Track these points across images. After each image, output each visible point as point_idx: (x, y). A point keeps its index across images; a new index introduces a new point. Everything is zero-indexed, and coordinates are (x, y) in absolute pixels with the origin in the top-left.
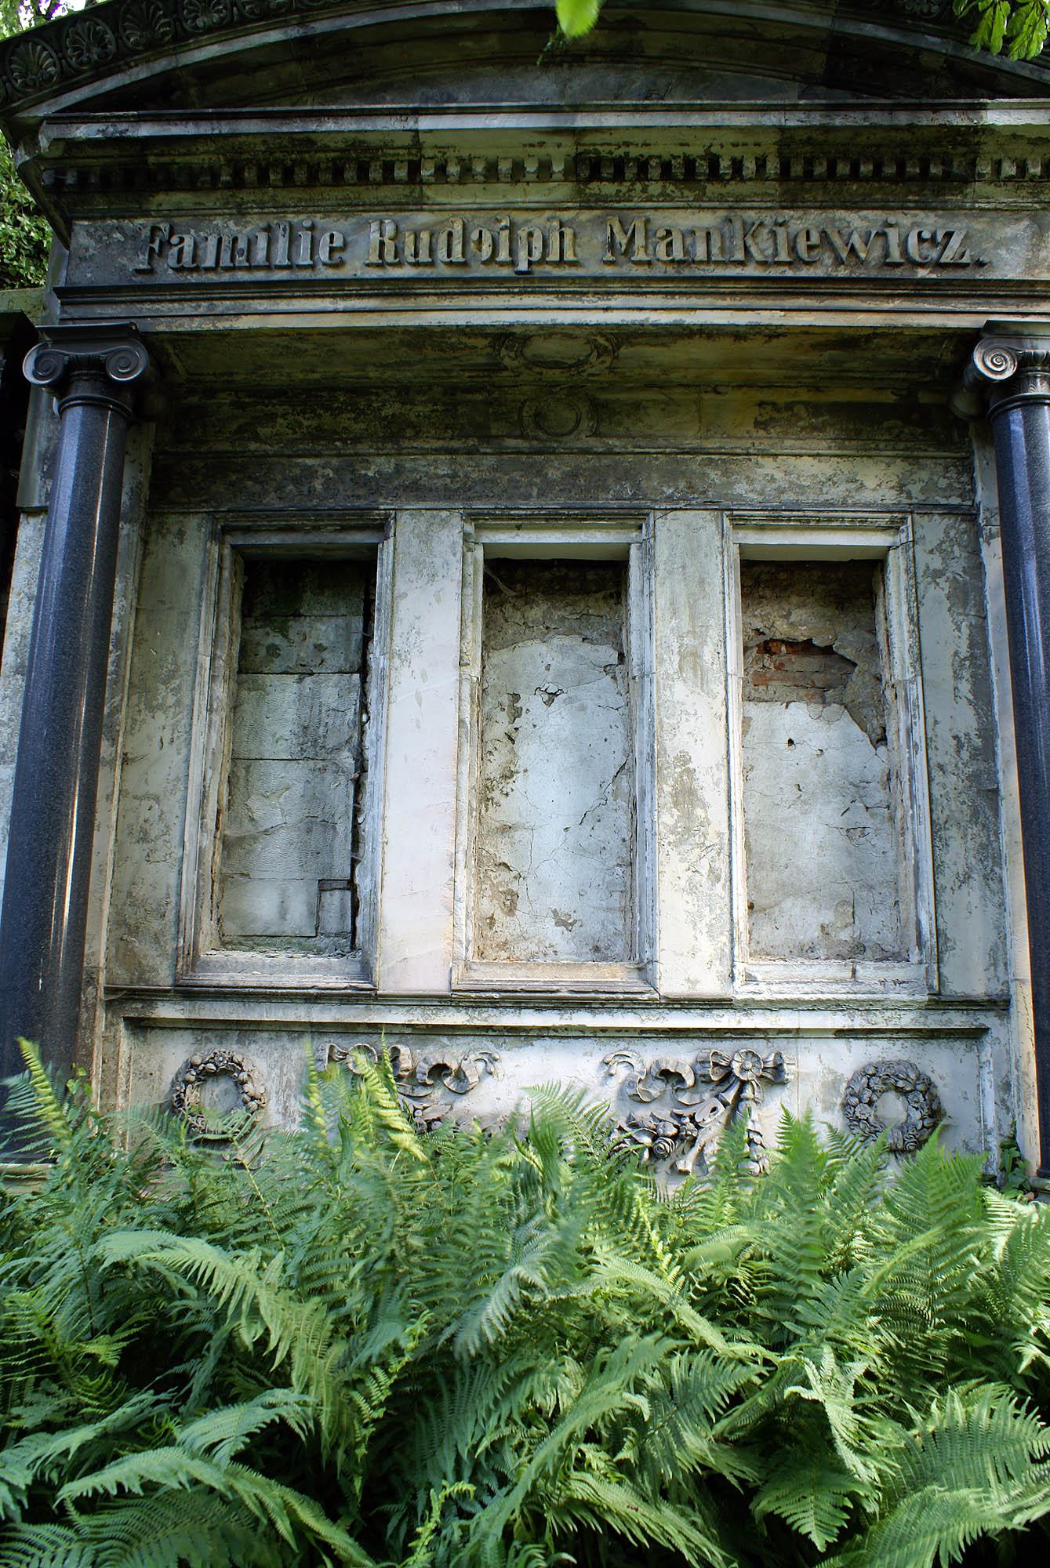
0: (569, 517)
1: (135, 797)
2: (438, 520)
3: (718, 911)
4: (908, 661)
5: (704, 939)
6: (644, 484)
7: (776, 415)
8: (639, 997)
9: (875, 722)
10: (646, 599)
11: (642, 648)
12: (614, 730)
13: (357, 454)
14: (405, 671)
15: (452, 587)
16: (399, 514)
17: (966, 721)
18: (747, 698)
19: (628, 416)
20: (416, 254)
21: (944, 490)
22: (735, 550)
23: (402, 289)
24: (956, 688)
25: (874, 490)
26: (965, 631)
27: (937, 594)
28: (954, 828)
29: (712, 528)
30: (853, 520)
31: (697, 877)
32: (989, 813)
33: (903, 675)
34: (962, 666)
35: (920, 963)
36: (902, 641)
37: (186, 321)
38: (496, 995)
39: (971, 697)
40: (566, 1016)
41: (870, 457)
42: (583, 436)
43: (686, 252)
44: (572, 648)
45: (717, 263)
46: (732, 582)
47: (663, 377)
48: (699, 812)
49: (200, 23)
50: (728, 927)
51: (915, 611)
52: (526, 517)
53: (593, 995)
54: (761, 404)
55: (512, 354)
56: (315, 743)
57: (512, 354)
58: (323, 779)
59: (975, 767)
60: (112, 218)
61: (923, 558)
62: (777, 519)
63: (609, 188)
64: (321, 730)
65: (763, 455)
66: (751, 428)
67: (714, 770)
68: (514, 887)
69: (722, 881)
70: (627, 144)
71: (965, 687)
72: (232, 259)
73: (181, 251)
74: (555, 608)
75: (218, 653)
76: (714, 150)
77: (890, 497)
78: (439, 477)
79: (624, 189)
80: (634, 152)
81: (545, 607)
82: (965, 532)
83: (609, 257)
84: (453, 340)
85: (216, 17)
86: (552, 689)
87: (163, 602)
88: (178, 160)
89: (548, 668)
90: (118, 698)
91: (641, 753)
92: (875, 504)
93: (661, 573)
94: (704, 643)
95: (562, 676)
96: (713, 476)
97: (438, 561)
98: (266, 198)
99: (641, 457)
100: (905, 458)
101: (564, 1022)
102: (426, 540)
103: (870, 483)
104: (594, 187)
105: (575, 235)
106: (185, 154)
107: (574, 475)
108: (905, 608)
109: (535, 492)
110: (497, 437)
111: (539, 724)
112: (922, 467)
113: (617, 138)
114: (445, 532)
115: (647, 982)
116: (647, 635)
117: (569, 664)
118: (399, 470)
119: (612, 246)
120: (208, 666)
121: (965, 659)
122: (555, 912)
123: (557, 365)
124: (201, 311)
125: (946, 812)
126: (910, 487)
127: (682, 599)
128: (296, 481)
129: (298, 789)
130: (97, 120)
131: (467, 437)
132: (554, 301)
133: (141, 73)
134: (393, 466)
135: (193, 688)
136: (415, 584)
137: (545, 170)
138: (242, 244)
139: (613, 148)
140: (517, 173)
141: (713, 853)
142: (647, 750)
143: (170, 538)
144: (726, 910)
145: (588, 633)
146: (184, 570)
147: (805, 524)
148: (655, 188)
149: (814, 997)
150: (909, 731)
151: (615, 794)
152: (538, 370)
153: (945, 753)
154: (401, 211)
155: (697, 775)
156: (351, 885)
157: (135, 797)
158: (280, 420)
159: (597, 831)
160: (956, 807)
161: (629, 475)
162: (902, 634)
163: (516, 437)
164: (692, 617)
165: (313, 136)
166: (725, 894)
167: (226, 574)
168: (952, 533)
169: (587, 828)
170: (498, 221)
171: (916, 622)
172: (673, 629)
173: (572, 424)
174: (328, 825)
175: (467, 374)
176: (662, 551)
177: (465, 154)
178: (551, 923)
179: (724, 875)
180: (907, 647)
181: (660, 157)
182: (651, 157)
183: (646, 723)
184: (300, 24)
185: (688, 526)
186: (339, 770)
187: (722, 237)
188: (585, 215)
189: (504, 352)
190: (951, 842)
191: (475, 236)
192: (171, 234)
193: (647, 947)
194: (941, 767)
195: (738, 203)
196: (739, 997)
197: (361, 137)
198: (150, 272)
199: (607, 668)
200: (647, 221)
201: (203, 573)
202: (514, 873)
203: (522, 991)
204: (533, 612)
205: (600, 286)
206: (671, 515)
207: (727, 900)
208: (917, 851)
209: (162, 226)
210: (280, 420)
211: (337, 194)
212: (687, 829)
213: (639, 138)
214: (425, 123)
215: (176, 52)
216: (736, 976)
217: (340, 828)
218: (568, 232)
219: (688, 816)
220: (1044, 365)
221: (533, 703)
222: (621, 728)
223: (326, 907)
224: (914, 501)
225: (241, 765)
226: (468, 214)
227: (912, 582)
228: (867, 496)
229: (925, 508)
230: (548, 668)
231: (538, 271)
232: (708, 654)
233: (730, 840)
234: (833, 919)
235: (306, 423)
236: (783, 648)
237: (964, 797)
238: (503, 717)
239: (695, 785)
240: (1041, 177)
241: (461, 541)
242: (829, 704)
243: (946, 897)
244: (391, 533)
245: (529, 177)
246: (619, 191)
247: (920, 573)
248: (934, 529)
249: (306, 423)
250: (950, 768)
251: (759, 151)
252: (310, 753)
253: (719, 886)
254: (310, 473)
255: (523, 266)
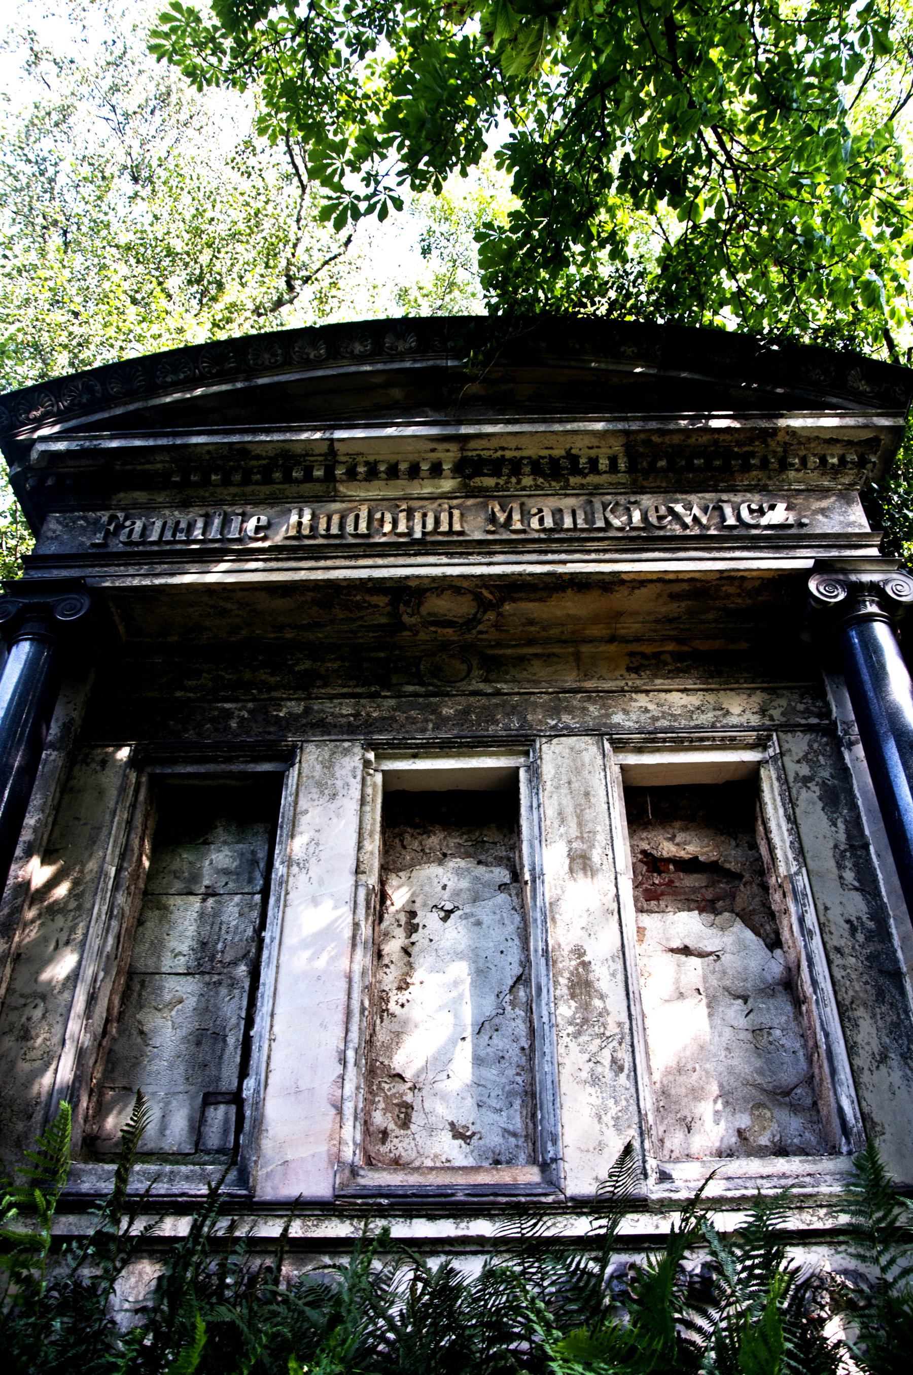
0: (461, 745)
1: (22, 996)
2: (340, 749)
3: (624, 1103)
4: (791, 856)
5: (610, 1133)
6: (529, 717)
7: (646, 663)
8: (543, 1199)
9: (768, 927)
10: (535, 811)
11: (532, 855)
12: (510, 943)
13: (271, 699)
14: (303, 878)
15: (351, 805)
16: (305, 745)
17: (856, 905)
18: (640, 910)
19: (514, 666)
20: (328, 529)
21: (803, 712)
22: (617, 769)
23: (315, 553)
24: (841, 877)
25: (739, 715)
26: (841, 826)
27: (809, 797)
28: (862, 1009)
29: (594, 750)
30: (723, 739)
31: (599, 1069)
32: (894, 991)
33: (788, 870)
34: (843, 857)
35: (850, 1153)
36: (783, 840)
37: (130, 579)
38: (385, 1201)
39: (856, 884)
40: (463, 1225)
41: (732, 690)
42: (474, 682)
43: (555, 523)
44: (468, 870)
45: (583, 530)
46: (616, 795)
47: (543, 634)
48: (597, 1003)
49: (169, 379)
50: (636, 1119)
51: (791, 811)
52: (422, 746)
53: (492, 1198)
54: (631, 654)
55: (409, 610)
56: (212, 958)
57: (409, 610)
58: (217, 993)
59: (872, 948)
60: (79, 511)
61: (792, 767)
62: (653, 741)
63: (490, 482)
64: (220, 946)
65: (636, 692)
66: (624, 672)
67: (610, 962)
68: (409, 1098)
69: (626, 1071)
70: (503, 449)
71: (849, 876)
72: (174, 535)
73: (131, 531)
74: (452, 837)
75: (125, 865)
76: (573, 451)
77: (755, 720)
78: (343, 716)
79: (502, 482)
80: (508, 454)
81: (442, 836)
82: (827, 744)
83: (491, 528)
84: (358, 598)
85: (182, 376)
86: (449, 906)
87: (78, 819)
88: (139, 467)
89: (444, 887)
90: (20, 900)
91: (536, 951)
92: (742, 726)
93: (548, 786)
94: (592, 846)
95: (458, 895)
96: (591, 709)
97: (339, 783)
98: (207, 494)
99: (526, 697)
100: (763, 690)
101: (460, 1233)
102: (328, 766)
103: (736, 710)
104: (478, 481)
105: (462, 515)
106: (144, 464)
107: (466, 712)
108: (781, 811)
109: (431, 726)
110: (396, 685)
111: (435, 939)
112: (779, 696)
113: (494, 443)
114: (347, 759)
115: (551, 1183)
116: (537, 842)
117: (464, 884)
118: (307, 711)
119: (493, 519)
120: (113, 874)
121: (845, 851)
122: (452, 1124)
123: (450, 624)
124: (142, 572)
125: (851, 993)
126: (771, 712)
127: (569, 810)
128: (213, 720)
129: (191, 1002)
130: (79, 439)
131: (370, 685)
132: (445, 560)
133: (119, 411)
134: (302, 708)
135: (96, 894)
136: (316, 803)
137: (436, 471)
138: (183, 525)
139: (491, 452)
140: (414, 472)
141: (615, 1043)
142: (541, 945)
143: (93, 765)
144: (632, 1102)
145: (483, 857)
146: (101, 793)
147: (679, 745)
148: (527, 481)
149: (738, 1193)
150: (801, 920)
151: (513, 1004)
152: (433, 629)
153: (840, 937)
154: (318, 502)
155: (593, 967)
156: (237, 1099)
157: (22, 996)
158: (204, 675)
159: (495, 1041)
160: (857, 987)
161: (514, 710)
162: (782, 834)
163: (414, 685)
164: (580, 824)
165: (249, 446)
166: (630, 1085)
167: (141, 797)
168: (815, 746)
169: (485, 1038)
170: (398, 506)
171: (792, 820)
172: (561, 836)
173: (464, 674)
174: (219, 1037)
175: (371, 634)
176: (548, 770)
177: (371, 459)
178: (447, 1136)
179: (627, 1066)
180: (788, 844)
181: (530, 458)
182: (523, 458)
183: (539, 922)
184: (245, 380)
185: (572, 749)
186: (233, 983)
187: (586, 513)
188: (470, 502)
189: (402, 608)
190: (861, 1022)
191: (378, 516)
192: (126, 519)
193: (550, 1146)
194: (838, 950)
195: (594, 491)
196: (654, 1197)
197: (287, 446)
198: (104, 545)
199: (502, 887)
200: (522, 505)
201: (119, 795)
202: (409, 1085)
203: (414, 1195)
204: (431, 840)
205: (483, 548)
206: (555, 741)
207: (633, 1090)
208: (827, 1035)
209: (119, 515)
210: (204, 675)
211: (266, 489)
212: (585, 1020)
213: (512, 443)
214: (340, 434)
215: (148, 398)
216: (649, 1172)
217: (231, 1040)
218: (456, 513)
219: (586, 1007)
220: (869, 591)
221: (430, 920)
222: (517, 941)
223: (209, 1119)
224: (777, 722)
225: (136, 979)
226: (372, 503)
227: (784, 787)
228: (734, 720)
229: (787, 727)
230: (444, 887)
231: (429, 538)
232: (596, 856)
233: (631, 1029)
234: (749, 1123)
235: (227, 677)
236: (671, 867)
237: (865, 978)
238: (400, 933)
239: (591, 977)
240: (839, 466)
241: (361, 767)
242: (720, 913)
243: (865, 1078)
244: (298, 760)
245: (422, 474)
246: (497, 484)
247: (791, 779)
248: (798, 744)
249: (227, 677)
250: (847, 951)
251: (609, 452)
252: (208, 967)
253: (623, 1076)
254: (228, 714)
255: (418, 535)
